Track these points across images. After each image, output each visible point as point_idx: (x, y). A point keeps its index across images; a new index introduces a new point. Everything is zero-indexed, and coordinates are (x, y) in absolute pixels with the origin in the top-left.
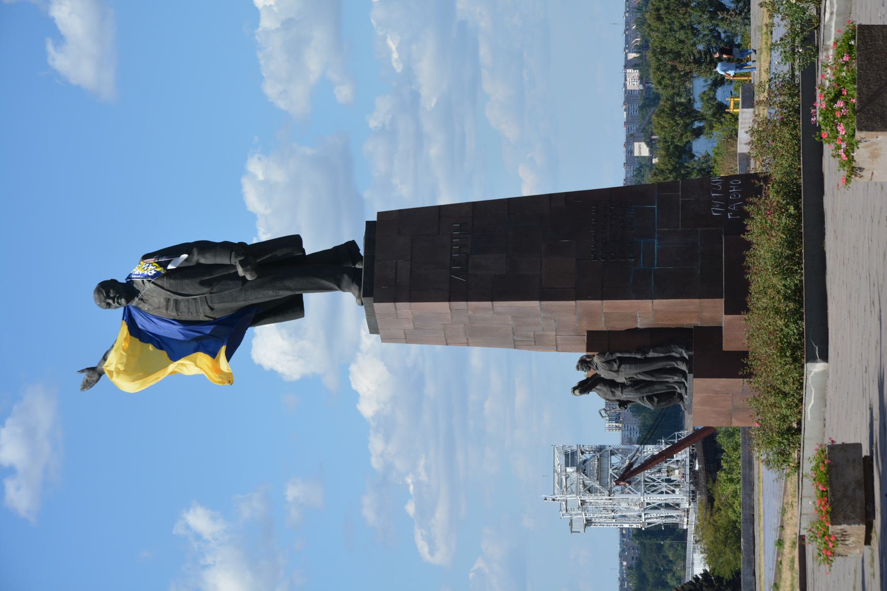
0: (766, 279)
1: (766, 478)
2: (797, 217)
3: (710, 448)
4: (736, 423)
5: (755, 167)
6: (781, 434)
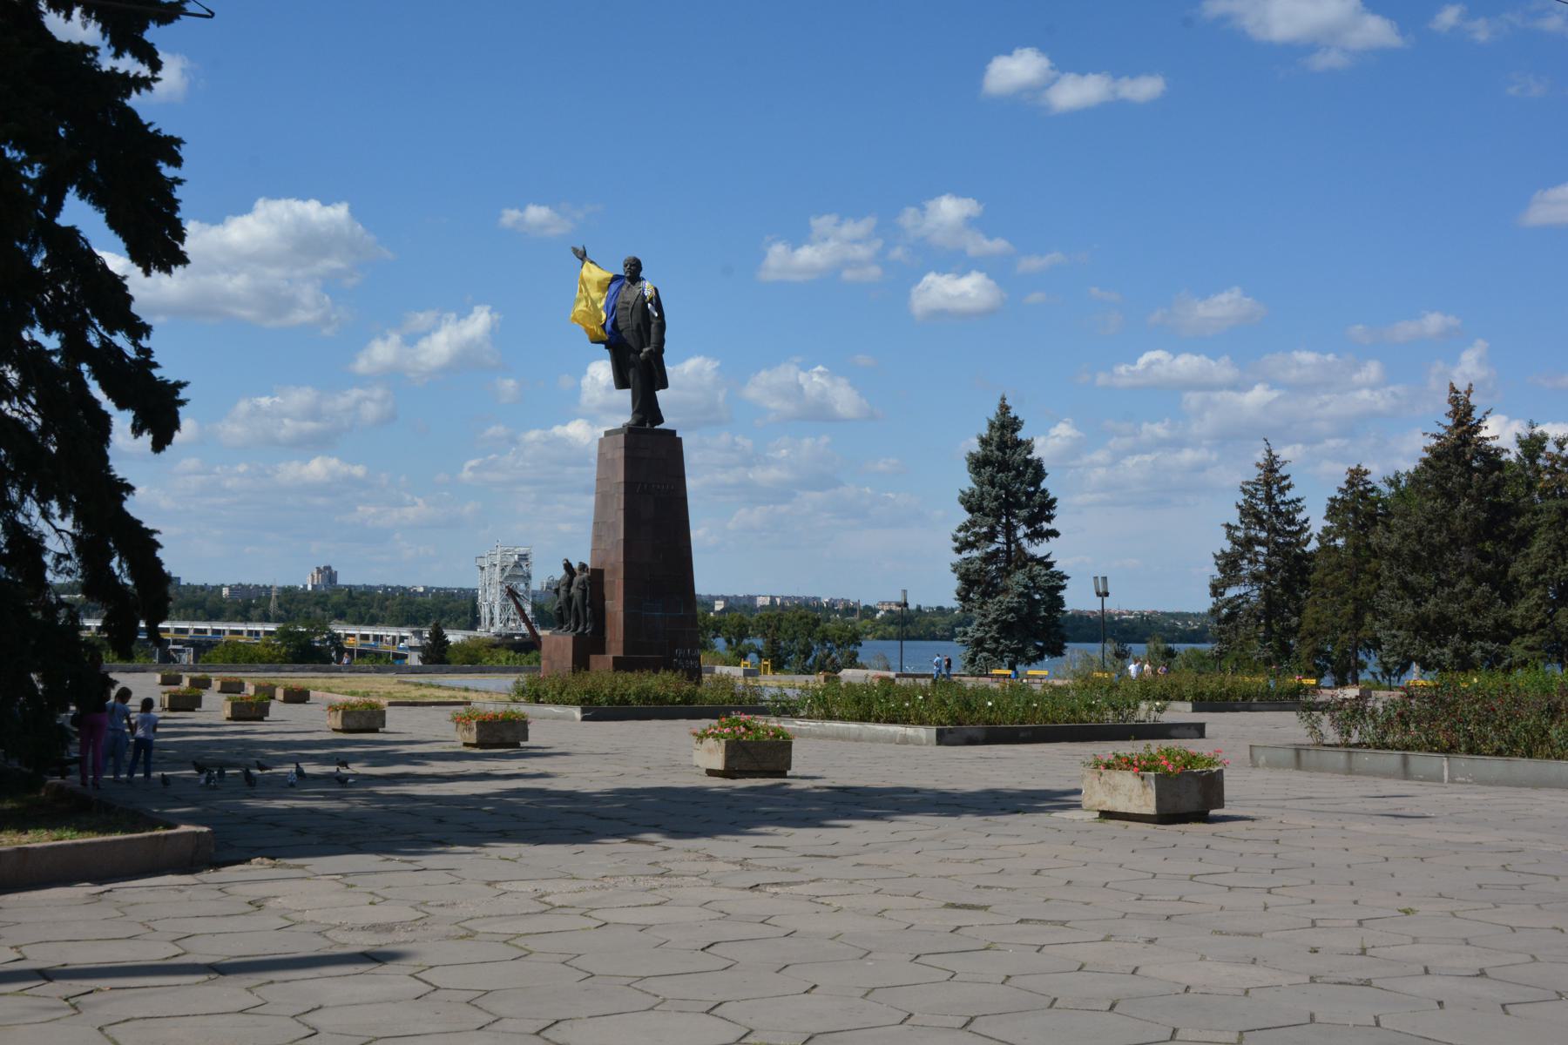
0: (635, 683)
1: (507, 682)
2: (673, 703)
3: (529, 645)
4: (543, 663)
5: (706, 677)
6: (536, 691)
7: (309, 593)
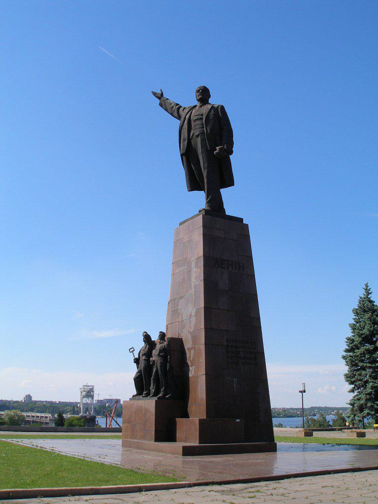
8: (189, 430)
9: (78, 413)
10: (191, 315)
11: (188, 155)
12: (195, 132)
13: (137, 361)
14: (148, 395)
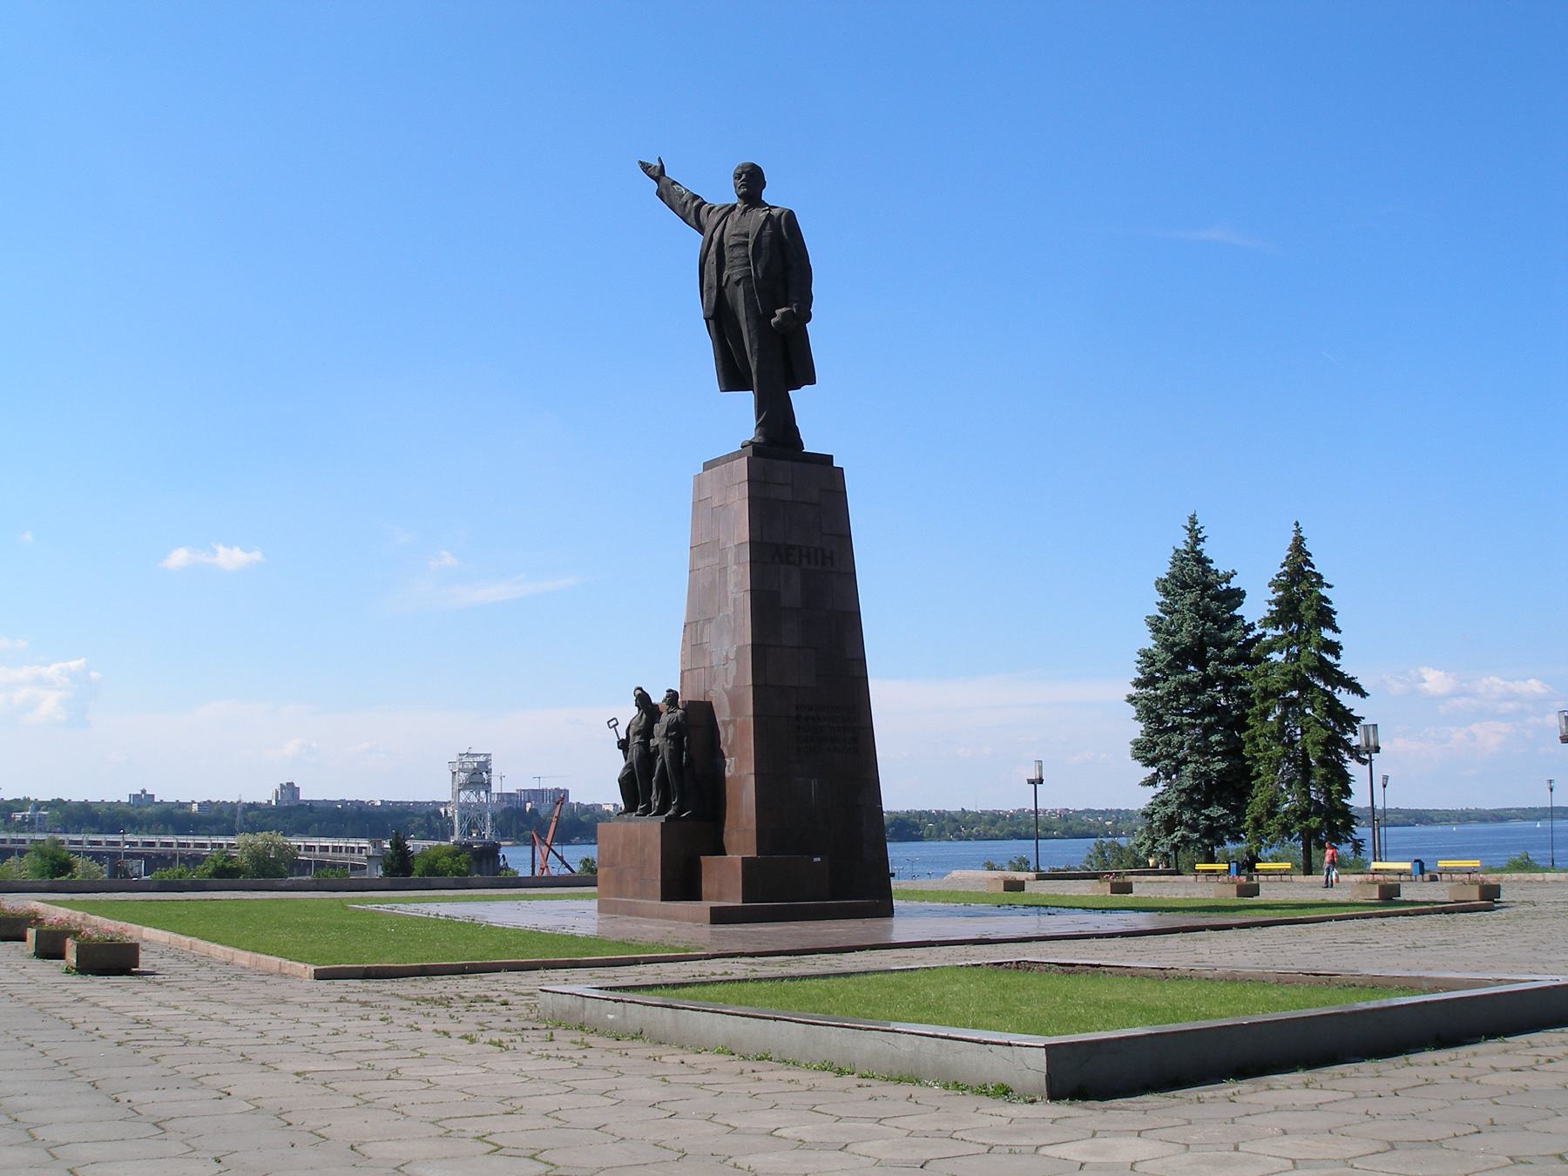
7: (273, 808)
8: (724, 878)
9: (445, 834)
10: (727, 657)
11: (720, 319)
12: (733, 273)
13: (623, 745)
14: (646, 811)
